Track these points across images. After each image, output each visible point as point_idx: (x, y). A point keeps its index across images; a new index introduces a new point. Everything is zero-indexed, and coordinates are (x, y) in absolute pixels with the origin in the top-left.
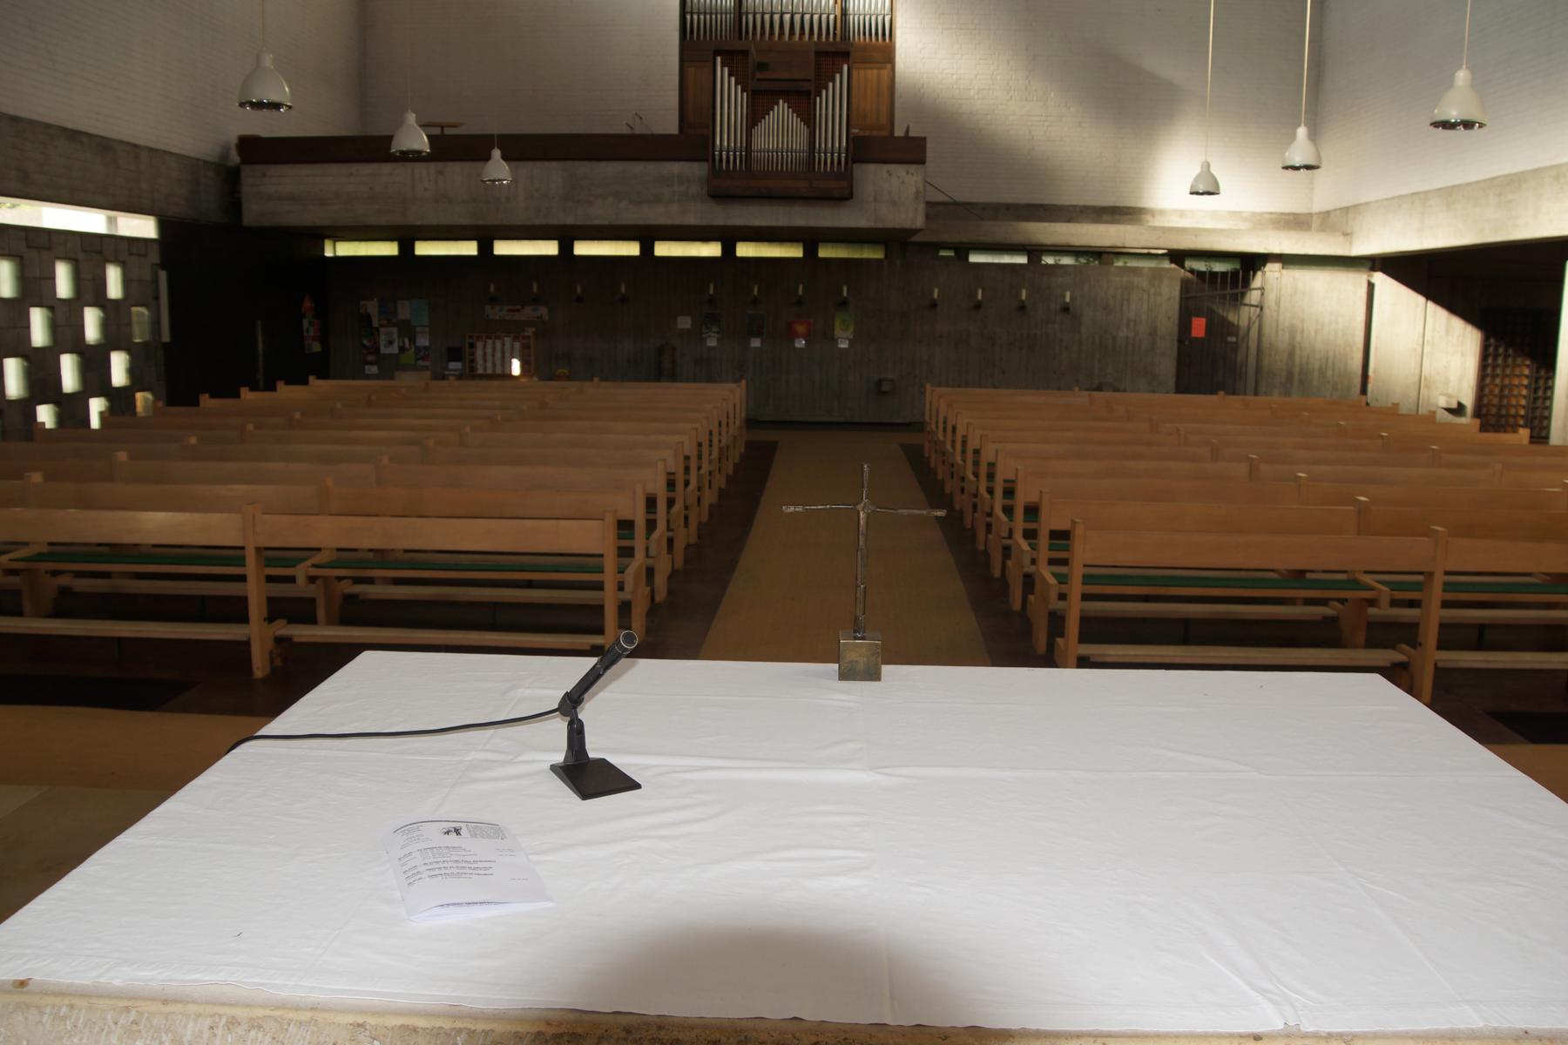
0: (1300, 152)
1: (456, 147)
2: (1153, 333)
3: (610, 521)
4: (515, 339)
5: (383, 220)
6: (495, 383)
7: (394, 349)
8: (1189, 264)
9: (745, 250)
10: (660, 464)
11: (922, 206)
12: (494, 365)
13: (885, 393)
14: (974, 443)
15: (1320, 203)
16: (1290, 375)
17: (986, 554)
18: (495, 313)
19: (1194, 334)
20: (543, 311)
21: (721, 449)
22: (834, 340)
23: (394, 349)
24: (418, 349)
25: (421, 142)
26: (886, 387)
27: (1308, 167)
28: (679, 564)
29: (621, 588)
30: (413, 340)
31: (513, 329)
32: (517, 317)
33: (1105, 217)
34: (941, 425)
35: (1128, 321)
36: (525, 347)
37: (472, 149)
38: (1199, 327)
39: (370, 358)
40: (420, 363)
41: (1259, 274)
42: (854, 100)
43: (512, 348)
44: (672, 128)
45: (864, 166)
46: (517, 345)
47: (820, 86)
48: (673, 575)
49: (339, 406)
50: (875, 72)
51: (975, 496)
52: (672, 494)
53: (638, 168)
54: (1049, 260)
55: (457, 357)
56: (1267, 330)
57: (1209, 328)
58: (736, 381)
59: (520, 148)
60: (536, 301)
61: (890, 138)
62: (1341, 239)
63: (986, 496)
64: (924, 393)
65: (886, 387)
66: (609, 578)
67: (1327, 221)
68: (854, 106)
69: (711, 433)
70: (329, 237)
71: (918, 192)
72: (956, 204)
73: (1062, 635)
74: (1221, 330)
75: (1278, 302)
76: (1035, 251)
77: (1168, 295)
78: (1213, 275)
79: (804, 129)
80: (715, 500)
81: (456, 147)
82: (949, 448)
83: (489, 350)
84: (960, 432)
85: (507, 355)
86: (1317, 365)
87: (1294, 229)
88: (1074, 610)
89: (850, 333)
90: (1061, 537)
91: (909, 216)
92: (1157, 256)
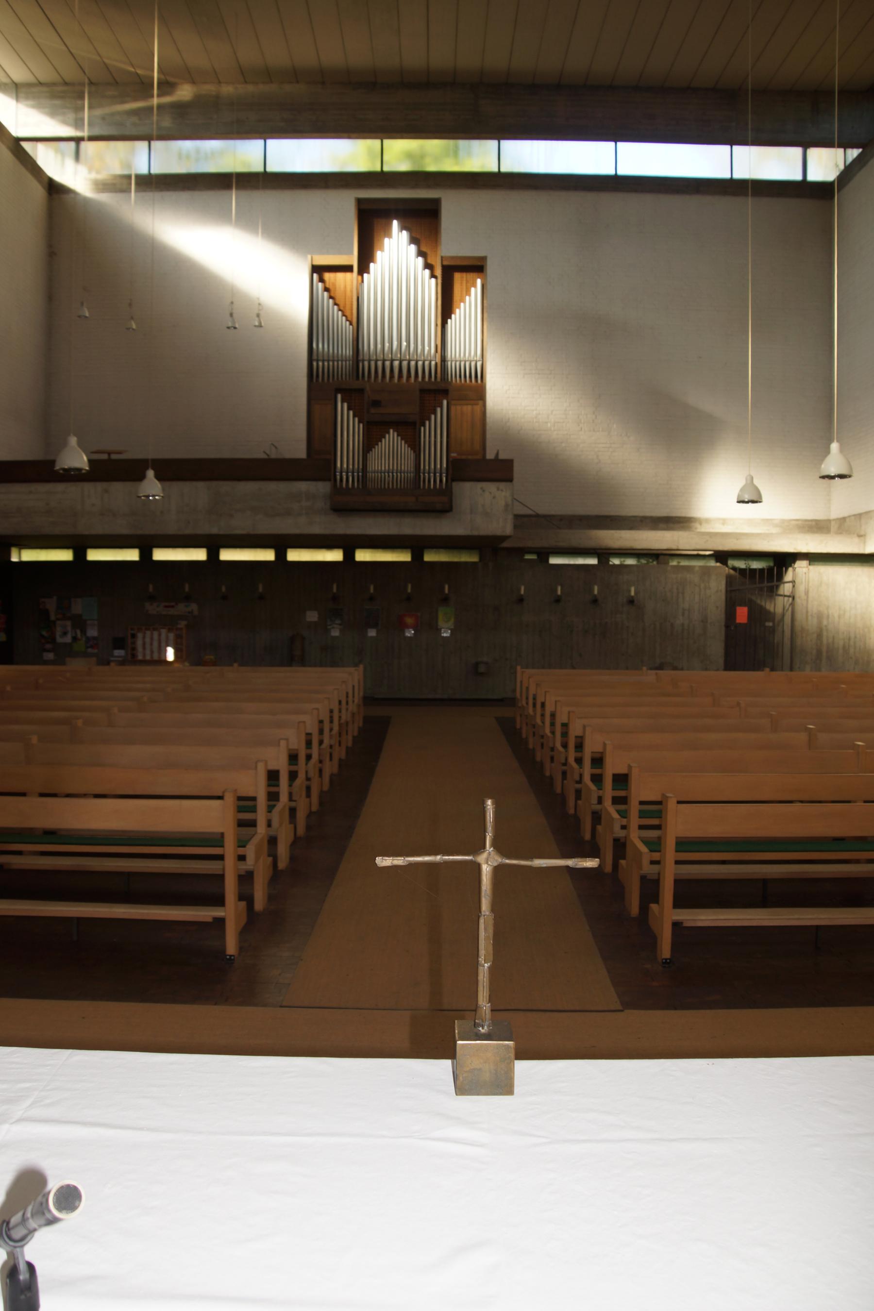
0: (833, 464)
1: (111, 469)
2: (704, 621)
3: (229, 798)
4: (170, 630)
5: (57, 531)
6: (149, 668)
7: (68, 639)
8: (732, 563)
9: (363, 556)
10: (283, 743)
11: (510, 517)
12: (152, 652)
13: (482, 674)
14: (562, 718)
15: (836, 512)
16: (819, 652)
17: (551, 778)
18: (152, 608)
19: (738, 621)
20: (194, 607)
21: (340, 725)
22: (438, 630)
23: (68, 639)
24: (88, 639)
25: (76, 458)
26: (482, 669)
27: (842, 476)
28: (301, 831)
29: (242, 858)
30: (84, 632)
31: (169, 623)
32: (172, 612)
33: (661, 525)
34: (531, 701)
35: (684, 610)
36: (178, 637)
37: (130, 471)
38: (742, 614)
39: (48, 646)
40: (90, 650)
41: (790, 569)
42: (452, 430)
43: (167, 638)
44: (301, 452)
45: (461, 484)
46: (171, 636)
47: (424, 417)
48: (296, 842)
49: (8, 688)
50: (469, 407)
51: (565, 764)
52: (294, 768)
53: (272, 486)
54: (616, 561)
55: (120, 646)
56: (799, 616)
57: (750, 615)
58: (356, 665)
59: (172, 470)
60: (188, 598)
61: (485, 460)
62: (856, 540)
63: (561, 749)
64: (515, 673)
65: (482, 669)
66: (230, 849)
67: (843, 526)
68: (452, 436)
69: (331, 711)
70: (15, 545)
71: (507, 505)
72: (537, 516)
73: (657, 901)
74: (759, 615)
75: (807, 593)
76: (603, 554)
77: (715, 590)
78: (753, 571)
79: (411, 454)
80: (335, 770)
81: (111, 469)
82: (538, 720)
83: (148, 640)
84: (549, 709)
85: (163, 644)
86: (841, 643)
87: (816, 532)
88: (669, 874)
89: (451, 624)
90: (621, 780)
91: (500, 525)
92: (704, 556)
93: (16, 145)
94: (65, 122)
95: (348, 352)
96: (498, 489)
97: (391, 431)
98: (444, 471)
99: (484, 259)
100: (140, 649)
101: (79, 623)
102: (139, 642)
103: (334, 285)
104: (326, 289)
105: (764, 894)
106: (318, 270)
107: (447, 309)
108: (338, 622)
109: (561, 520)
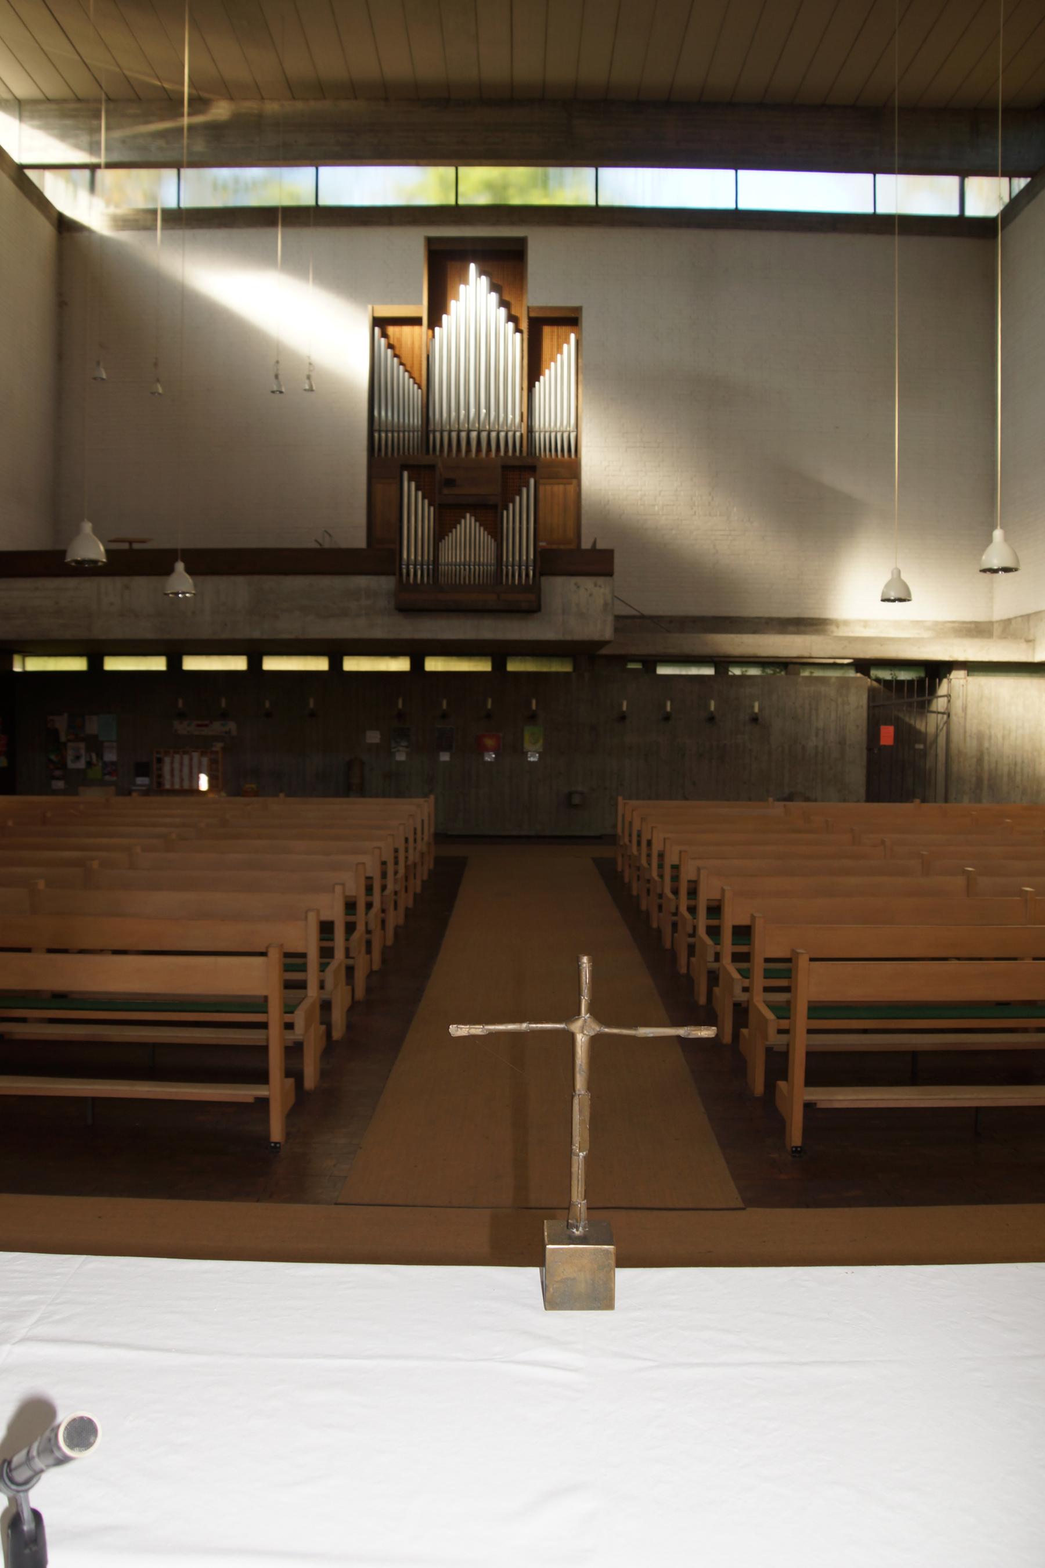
0: (996, 554)
1: (133, 561)
2: (842, 742)
3: (274, 955)
4: (203, 754)
5: (68, 635)
6: (178, 799)
7: (81, 764)
8: (875, 673)
9: (433, 665)
10: (338, 889)
11: (610, 618)
12: (182, 780)
13: (576, 806)
14: (672, 859)
15: (999, 613)
16: (979, 780)
17: (659, 930)
18: (182, 728)
19: (882, 743)
20: (232, 726)
21: (407, 867)
22: (524, 754)
23: (81, 764)
24: (105, 765)
25: (91, 548)
26: (576, 800)
27: (1006, 570)
28: (360, 994)
29: (289, 1026)
30: (100, 756)
31: (202, 745)
32: (205, 731)
33: (791, 628)
34: (635, 839)
35: (817, 729)
36: (213, 762)
37: (155, 563)
38: (887, 735)
39: (58, 773)
40: (107, 778)
41: (945, 681)
42: (541, 514)
43: (200, 763)
44: (360, 541)
45: (551, 579)
46: (205, 760)
47: (507, 499)
48: (354, 1007)
49: (10, 823)
50: (561, 487)
51: (675, 914)
52: (351, 919)
53: (325, 582)
54: (736, 671)
55: (144, 772)
56: (955, 737)
57: (897, 736)
58: (426, 796)
59: (205, 563)
60: (224, 716)
61: (580, 550)
62: (1024, 645)
63: (671, 896)
64: (616, 804)
65: (576, 800)
66: (274, 1016)
67: (1008, 629)
68: (541, 521)
69: (396, 851)
70: (18, 652)
71: (606, 605)
72: (642, 617)
73: (785, 1078)
74: (908, 736)
75: (965, 709)
76: (721, 662)
77: (855, 705)
78: (900, 683)
79: (491, 543)
80: (401, 921)
81: (133, 561)
82: (644, 862)
83: (177, 765)
84: (656, 848)
85: (195, 770)
86: (1006, 769)
87: (976, 637)
88: (800, 1045)
89: (539, 746)
90: (743, 933)
91: (598, 628)
92: (842, 665)
93: (19, 173)
94: (78, 146)
95: (417, 421)
96: (596, 585)
97: (468, 515)
98: (531, 563)
99: (579, 309)
100: (167, 776)
101: (95, 745)
102: (167, 768)
103: (399, 340)
104: (390, 346)
105: (914, 1069)
106: (380, 323)
107: (534, 369)
108: (404, 744)
109: (671, 622)
